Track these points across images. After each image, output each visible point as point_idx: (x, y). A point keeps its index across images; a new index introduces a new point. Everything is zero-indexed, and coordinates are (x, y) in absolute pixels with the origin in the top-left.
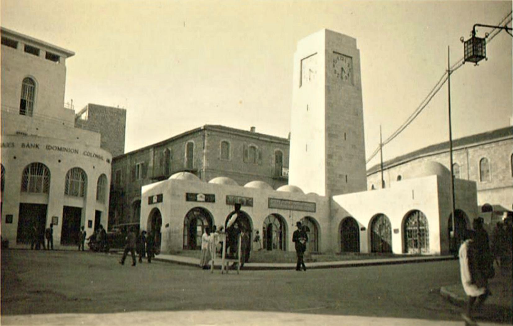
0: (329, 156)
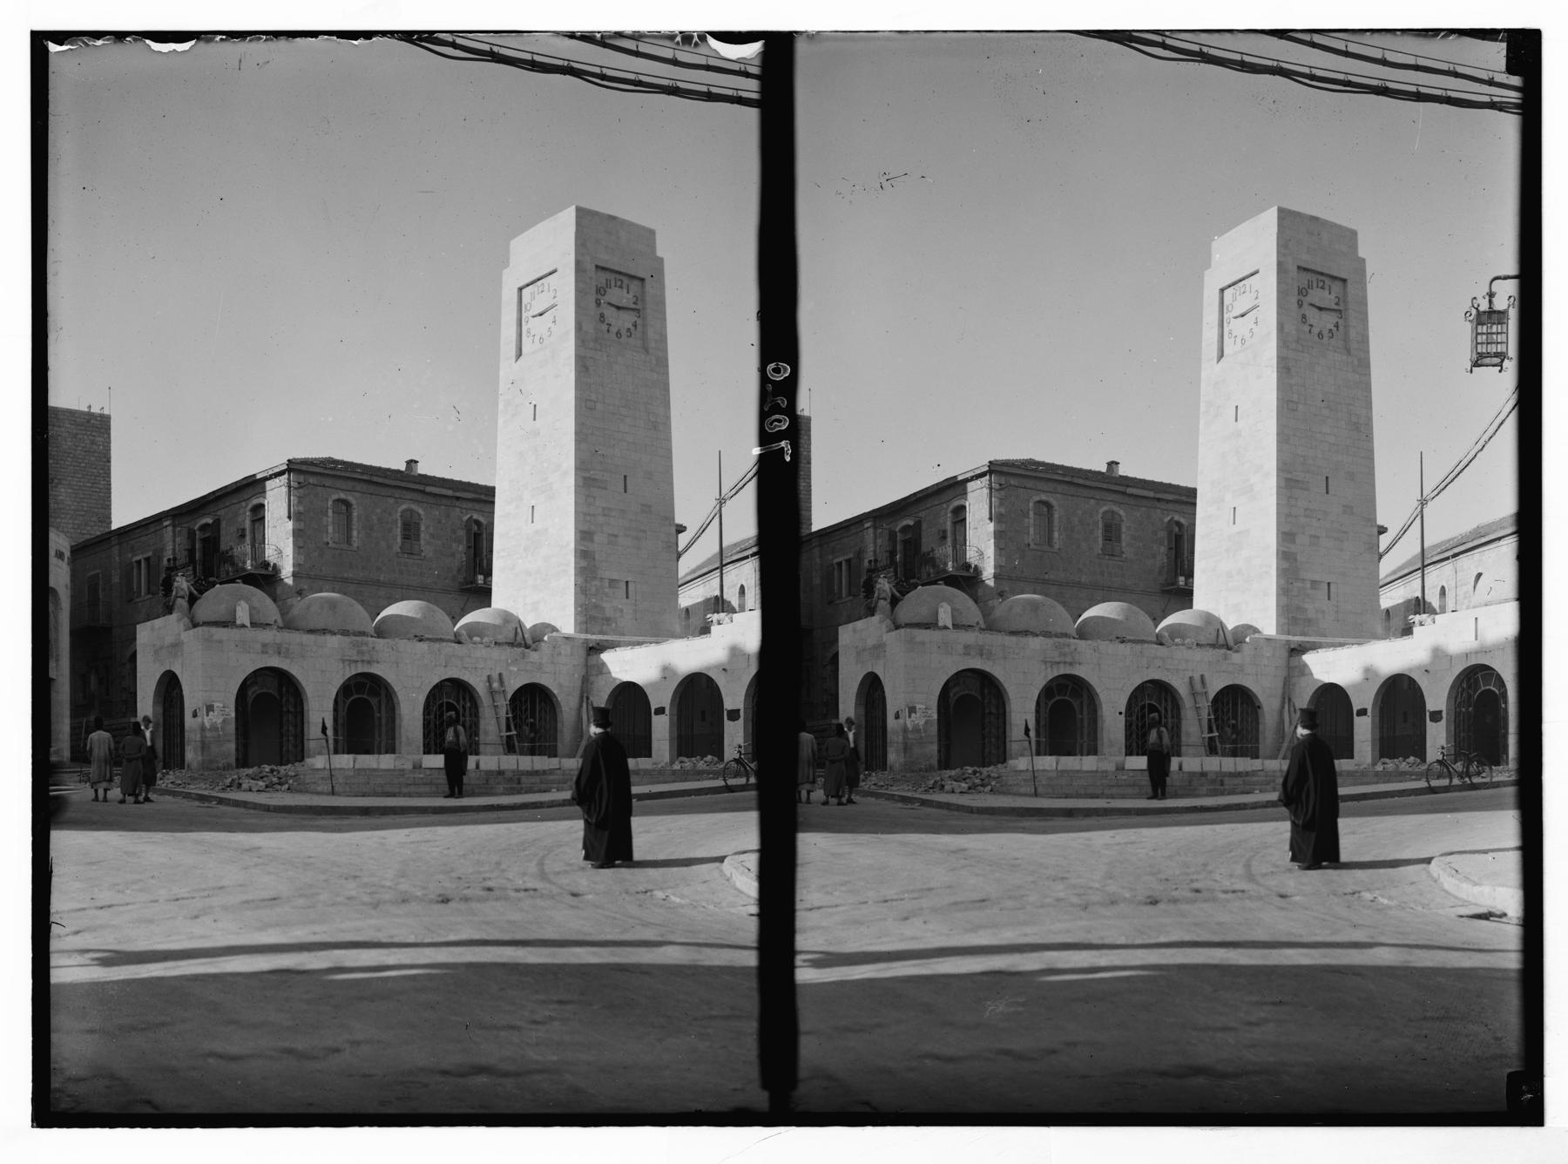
0: (1286, 536)
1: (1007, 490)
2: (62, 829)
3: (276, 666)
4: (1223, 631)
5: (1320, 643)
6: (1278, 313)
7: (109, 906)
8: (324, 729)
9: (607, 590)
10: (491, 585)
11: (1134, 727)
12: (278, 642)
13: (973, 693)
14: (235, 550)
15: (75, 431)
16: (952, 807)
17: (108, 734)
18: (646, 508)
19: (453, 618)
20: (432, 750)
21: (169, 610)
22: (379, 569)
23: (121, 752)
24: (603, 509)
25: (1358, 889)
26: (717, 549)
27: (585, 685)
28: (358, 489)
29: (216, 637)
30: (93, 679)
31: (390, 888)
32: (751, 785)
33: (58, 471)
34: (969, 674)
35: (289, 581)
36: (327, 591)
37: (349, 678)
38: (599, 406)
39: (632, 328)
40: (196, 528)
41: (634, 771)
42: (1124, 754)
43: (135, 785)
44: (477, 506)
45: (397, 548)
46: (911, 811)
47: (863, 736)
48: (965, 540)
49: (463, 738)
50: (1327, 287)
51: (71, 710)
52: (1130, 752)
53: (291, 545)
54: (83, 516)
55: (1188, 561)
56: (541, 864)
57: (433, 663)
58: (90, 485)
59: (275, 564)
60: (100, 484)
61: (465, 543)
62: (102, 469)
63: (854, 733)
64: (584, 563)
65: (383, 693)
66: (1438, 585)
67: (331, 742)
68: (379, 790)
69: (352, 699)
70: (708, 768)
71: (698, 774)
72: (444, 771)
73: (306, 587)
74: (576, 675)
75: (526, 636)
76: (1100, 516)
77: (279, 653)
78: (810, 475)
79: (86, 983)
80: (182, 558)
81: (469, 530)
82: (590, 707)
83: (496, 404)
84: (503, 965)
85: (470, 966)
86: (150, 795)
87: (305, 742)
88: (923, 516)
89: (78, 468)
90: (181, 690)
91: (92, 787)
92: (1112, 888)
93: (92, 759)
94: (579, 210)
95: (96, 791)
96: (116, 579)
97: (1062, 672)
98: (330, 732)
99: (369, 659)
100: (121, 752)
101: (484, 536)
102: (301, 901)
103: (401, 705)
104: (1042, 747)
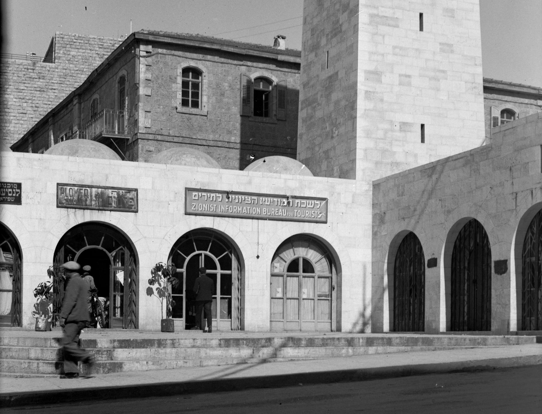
24: (394, 47)
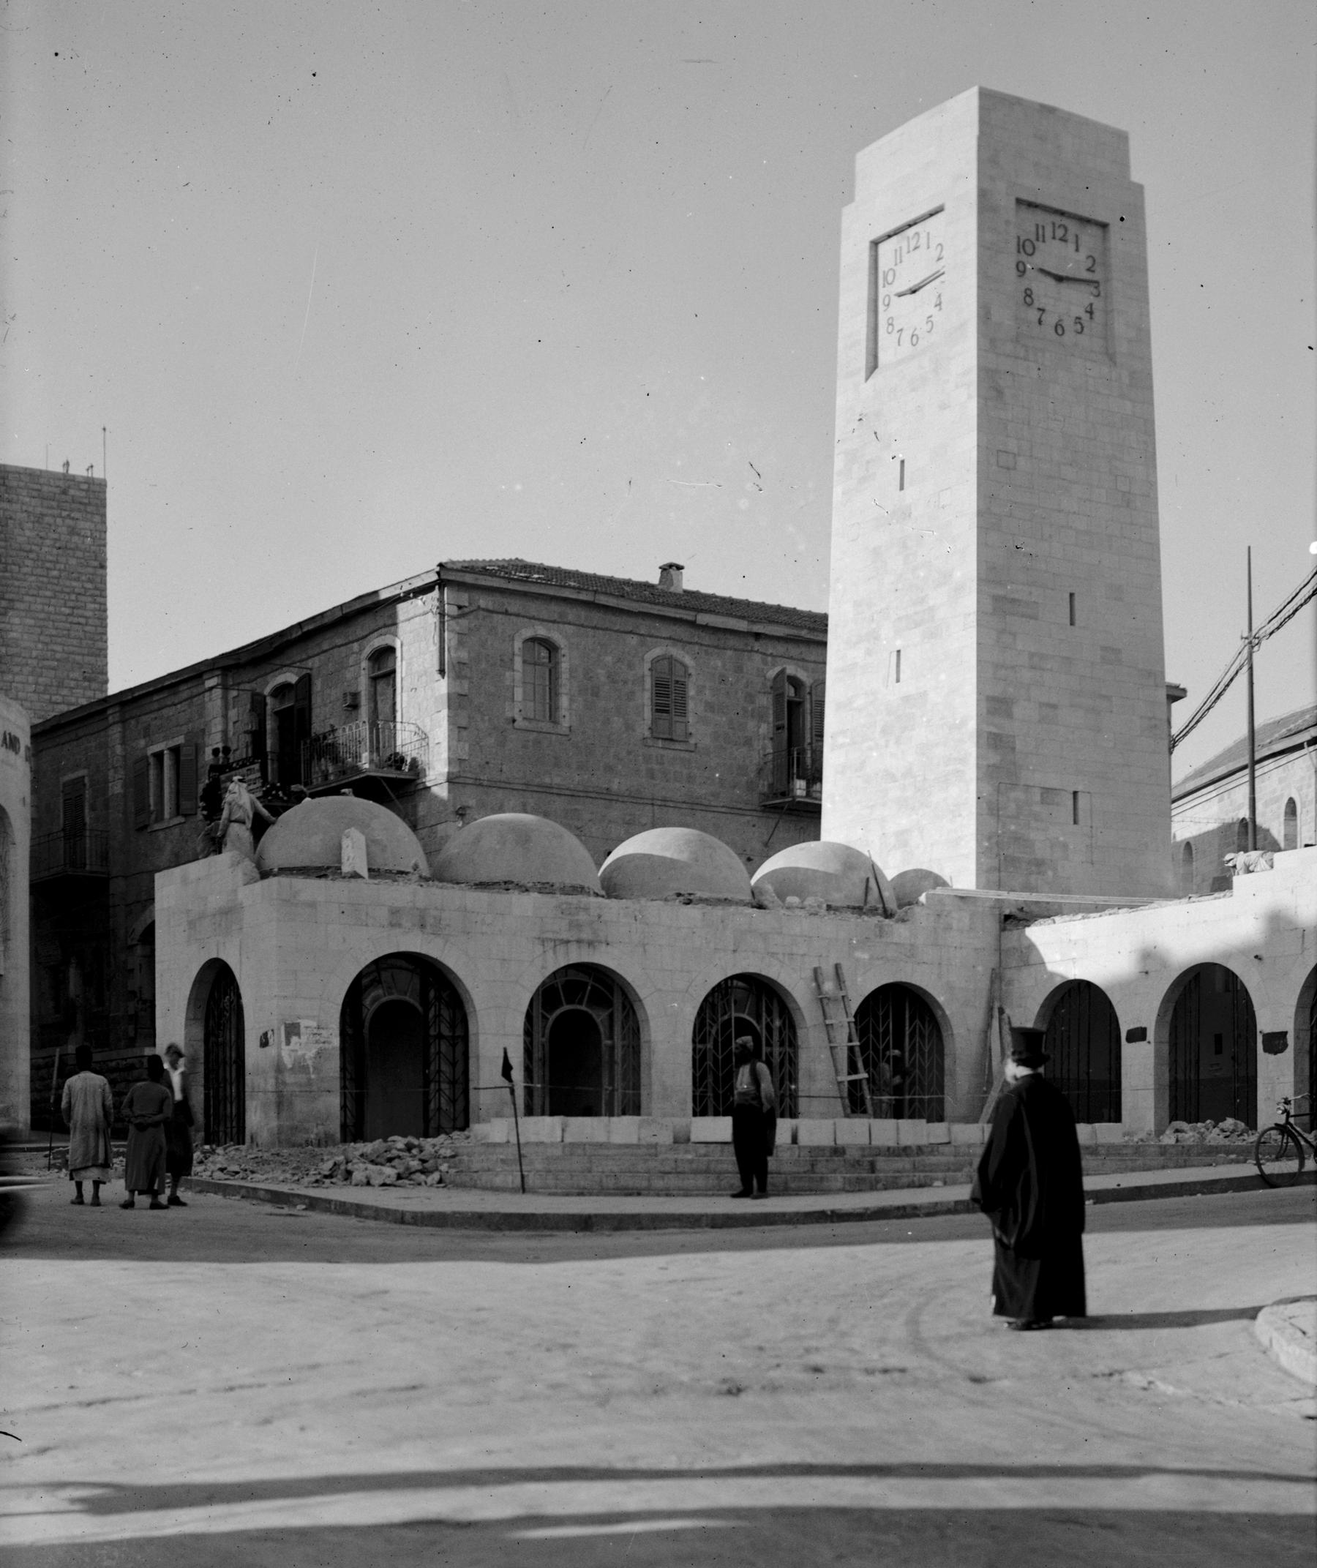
1: (471, 617)
2: (15, 1256)
3: (418, 951)
4: (876, 879)
5: (1060, 904)
6: (979, 287)
7: (104, 1402)
8: (507, 1069)
9: (1037, 808)
10: (820, 800)
11: (709, 1063)
12: (420, 905)
13: (407, 998)
14: (340, 731)
15: (39, 510)
16: (365, 1213)
17: (101, 1077)
18: (1111, 654)
19: (749, 859)
20: (711, 1109)
21: (216, 845)
22: (609, 769)
23: (126, 1111)
24: (1032, 655)
25: (1118, 1365)
26: (1244, 731)
27: (996, 986)
28: (571, 618)
29: (304, 897)
30: (73, 975)
31: (630, 1366)
32: (1309, 1173)
33: (7, 586)
34: (403, 964)
35: (442, 791)
36: (513, 810)
37: (554, 973)
38: (1022, 462)
39: (1085, 317)
40: (267, 691)
41: (1087, 1148)
42: (690, 1112)
43: (153, 1175)
44: (794, 650)
45: (643, 729)
46: (289, 1219)
47: (200, 1079)
48: (394, 711)
49: (767, 1086)
50: (1071, 237)
51: (33, 1032)
52: (701, 1109)
53: (445, 724)
54: (54, 669)
55: (813, 752)
56: (913, 1322)
57: (712, 945)
58: (67, 611)
59: (414, 761)
60: (84, 608)
61: (771, 719)
62: (90, 581)
63: (183, 1074)
64: (994, 758)
65: (617, 1001)
66: (1282, 795)
67: (520, 1092)
68: (610, 1183)
69: (558, 1012)
70: (1227, 1142)
71: (1209, 1154)
72: (731, 1149)
73: (472, 802)
74: (980, 968)
75: (886, 894)
76: (647, 665)
77: (423, 926)
78: (104, 590)
79: (61, 1546)
80: (241, 748)
81: (778, 697)
82: (1006, 1028)
83: (830, 458)
84: (843, 1512)
85: (780, 1513)
86: (181, 1193)
87: (472, 1093)
88: (316, 665)
89: (45, 580)
90: (239, 997)
91: (72, 1179)
92: (657, 1363)
93: (71, 1125)
94: (985, 95)
95: (79, 1185)
96: (116, 788)
97: (574, 959)
98: (518, 1074)
99: (591, 937)
100: (126, 1111)
101: (808, 706)
102: (464, 1393)
103: (652, 1024)
104: (537, 1101)
